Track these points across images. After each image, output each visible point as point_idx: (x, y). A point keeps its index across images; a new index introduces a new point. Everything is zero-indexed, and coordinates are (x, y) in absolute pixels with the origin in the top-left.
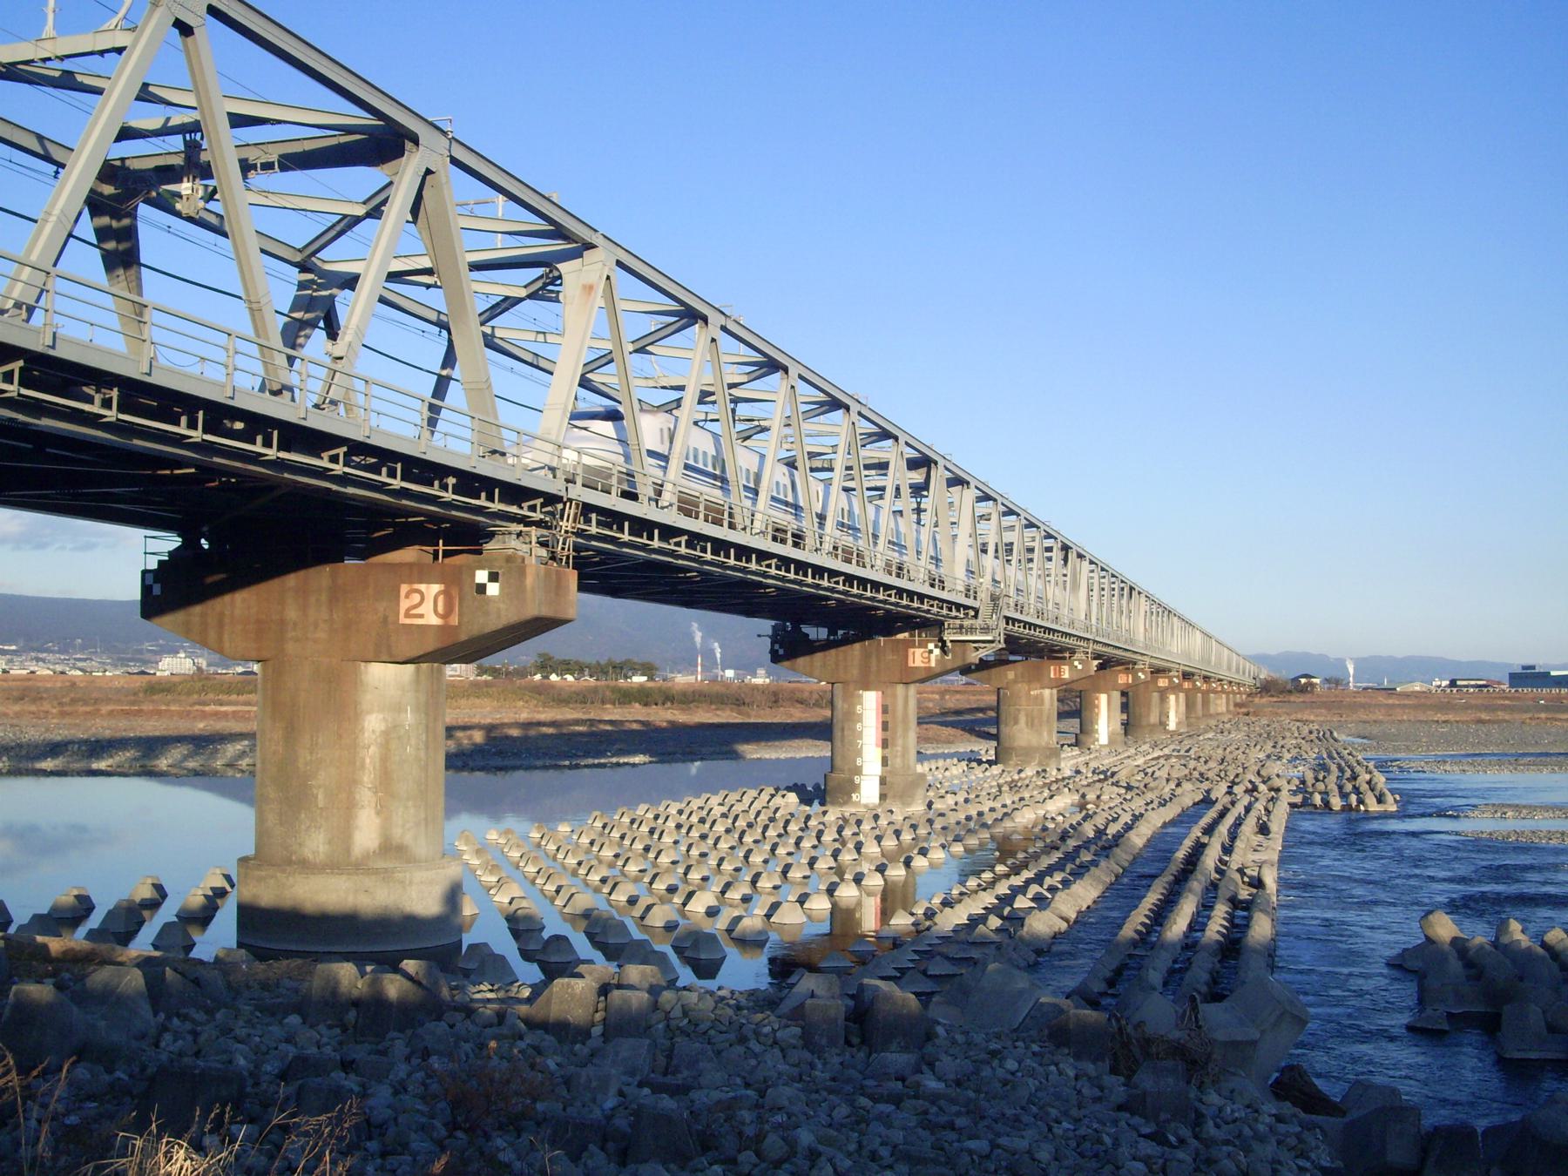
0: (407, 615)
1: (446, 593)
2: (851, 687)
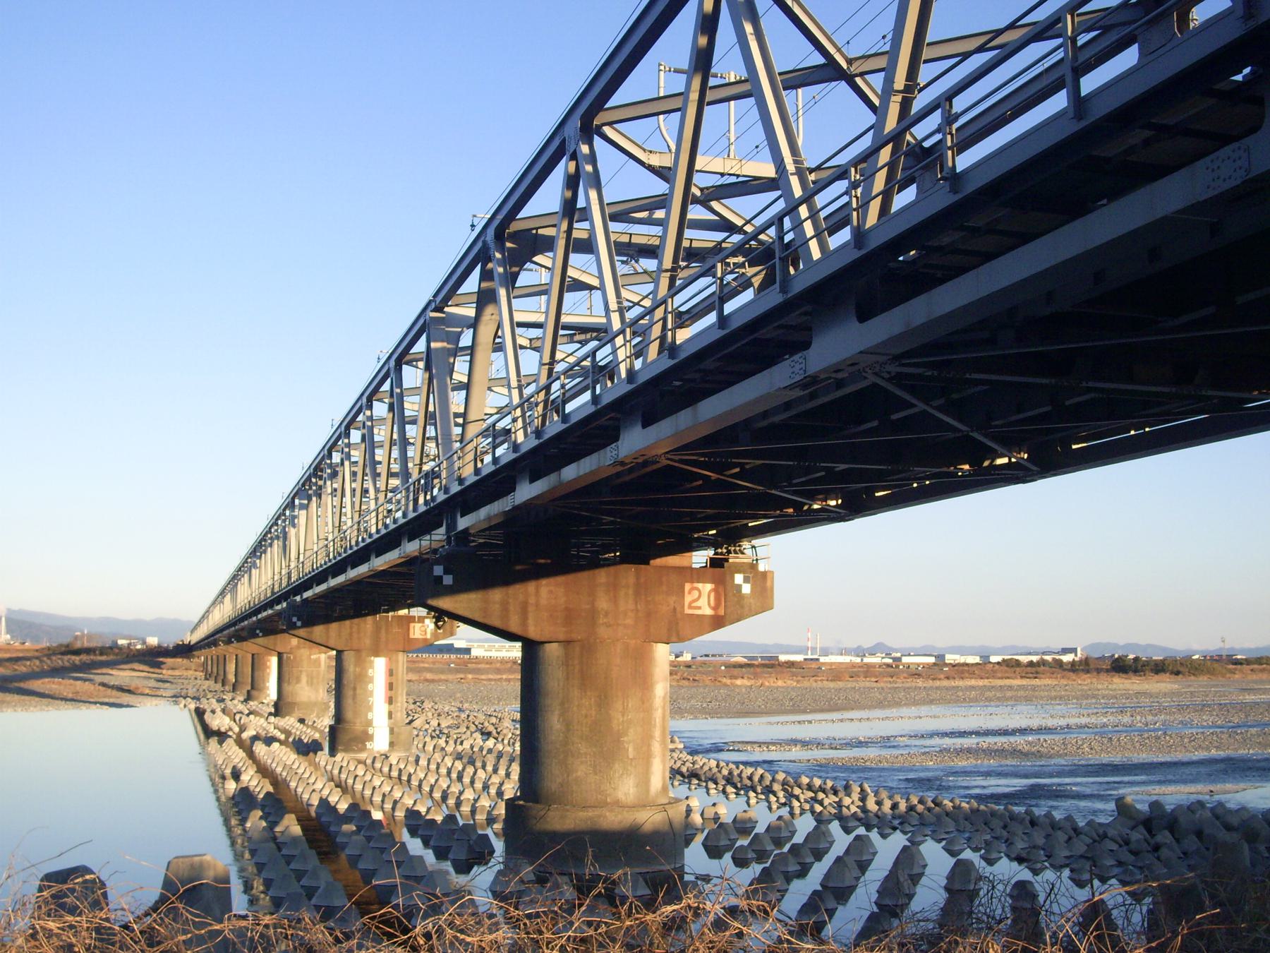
0: (690, 607)
1: (715, 590)
2: (364, 654)
